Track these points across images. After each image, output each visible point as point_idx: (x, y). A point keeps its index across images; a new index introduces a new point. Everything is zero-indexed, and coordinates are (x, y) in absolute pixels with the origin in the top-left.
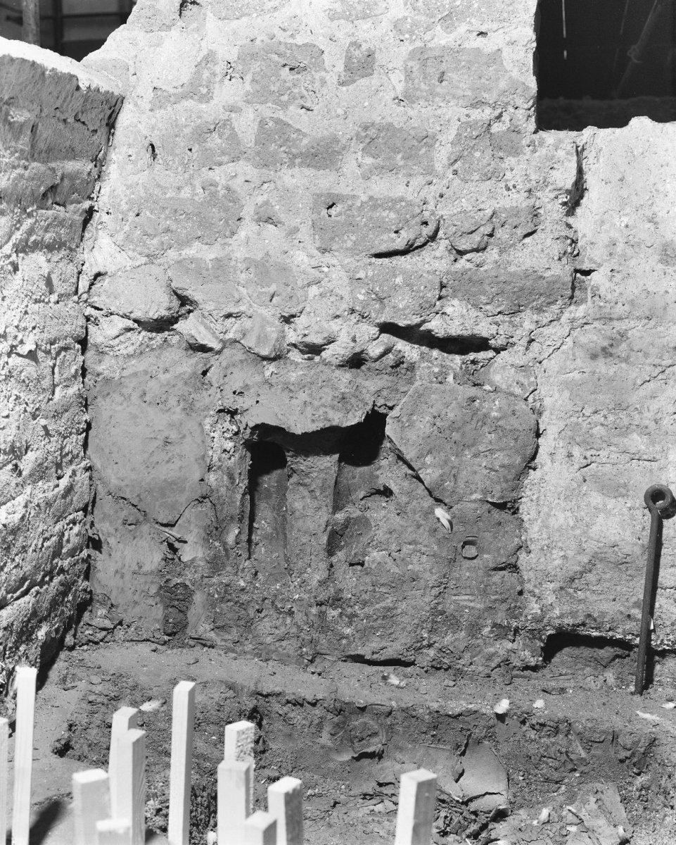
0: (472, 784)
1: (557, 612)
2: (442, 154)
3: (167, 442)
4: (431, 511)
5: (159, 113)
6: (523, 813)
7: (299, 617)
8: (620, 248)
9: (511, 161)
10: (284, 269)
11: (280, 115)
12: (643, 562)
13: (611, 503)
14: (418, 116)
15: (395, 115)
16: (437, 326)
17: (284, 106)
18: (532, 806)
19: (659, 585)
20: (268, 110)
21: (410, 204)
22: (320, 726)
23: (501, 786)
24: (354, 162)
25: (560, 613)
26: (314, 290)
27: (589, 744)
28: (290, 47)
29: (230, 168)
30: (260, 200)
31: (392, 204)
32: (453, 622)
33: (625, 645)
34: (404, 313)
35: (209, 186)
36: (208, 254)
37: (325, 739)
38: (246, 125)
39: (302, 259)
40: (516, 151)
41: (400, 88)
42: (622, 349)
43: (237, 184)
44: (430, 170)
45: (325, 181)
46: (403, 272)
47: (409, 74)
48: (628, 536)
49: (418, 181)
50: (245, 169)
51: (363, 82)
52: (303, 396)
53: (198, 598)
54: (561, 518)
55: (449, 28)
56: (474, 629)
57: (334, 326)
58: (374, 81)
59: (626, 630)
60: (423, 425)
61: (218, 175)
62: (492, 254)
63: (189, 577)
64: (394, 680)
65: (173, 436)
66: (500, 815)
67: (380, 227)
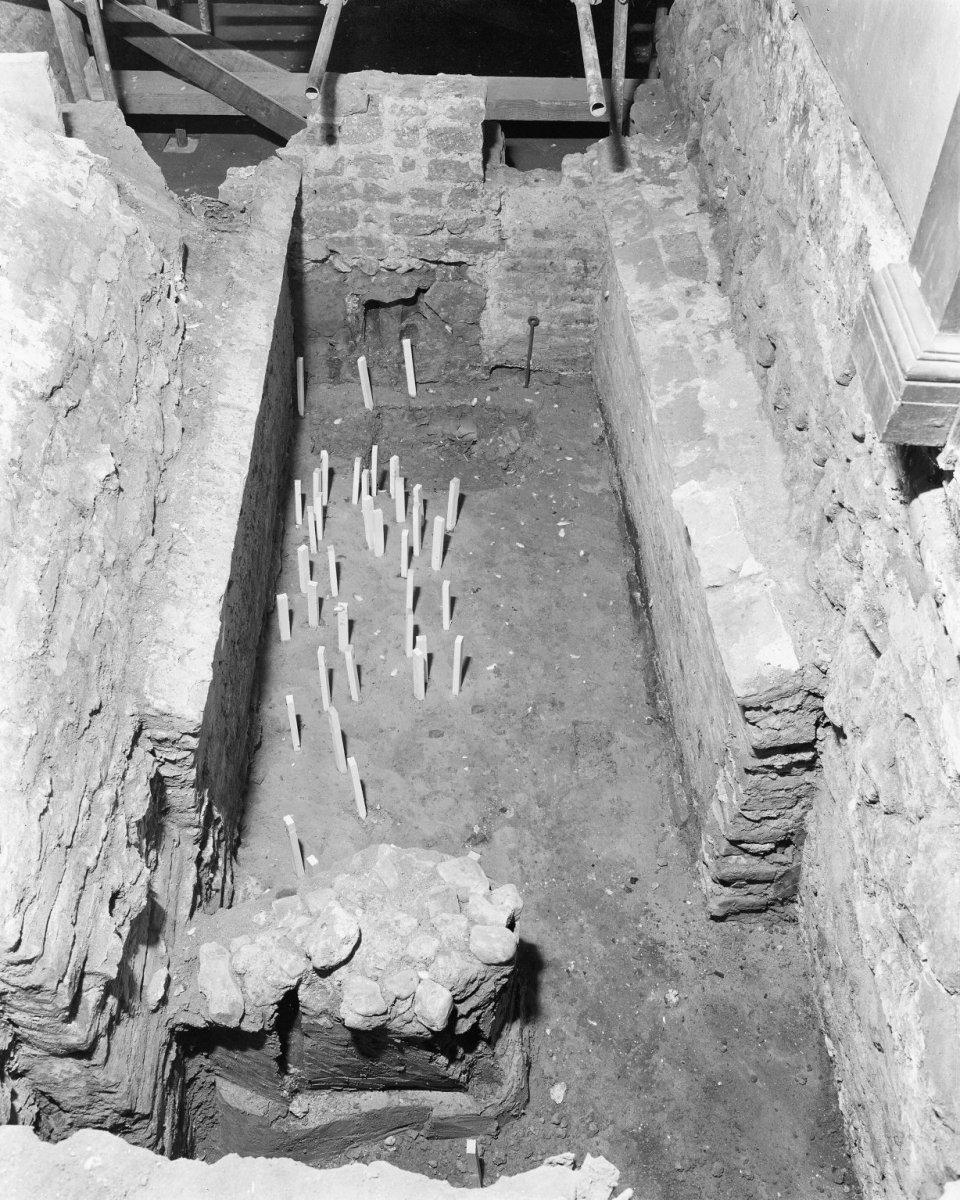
0: (463, 430)
1: (495, 360)
2: (445, 199)
3: (328, 307)
4: (443, 327)
5: (318, 179)
6: (483, 440)
7: (390, 369)
8: (517, 232)
9: (473, 200)
10: (379, 241)
11: (374, 182)
12: (528, 341)
13: (515, 321)
14: (435, 185)
15: (426, 185)
16: (444, 259)
17: (377, 179)
18: (487, 437)
19: (233, 1024)
20: (370, 180)
21: (432, 218)
22: (403, 416)
23: (475, 430)
24: (408, 201)
25: (496, 361)
26: (392, 248)
27: (506, 414)
28: (377, 156)
29: (353, 201)
30: (367, 213)
31: (425, 218)
32: (454, 365)
33: (523, 369)
34: (431, 254)
35: (343, 208)
36: (344, 235)
37: (406, 419)
38: (359, 185)
39: (386, 236)
40: (476, 197)
41: (426, 175)
42: (519, 267)
43: (356, 208)
44: (440, 206)
45: (396, 208)
46: (430, 243)
47: (430, 169)
48: (521, 332)
49: (434, 210)
50: (359, 202)
51: (410, 172)
52: (388, 288)
53: (345, 364)
54: (496, 327)
55: (446, 153)
56: (462, 367)
57: (401, 261)
58: (415, 171)
59: (523, 365)
60: (440, 297)
61: (346, 204)
62: (467, 234)
63: (340, 356)
64: (431, 391)
65: (331, 304)
66: (474, 443)
67: (420, 225)
